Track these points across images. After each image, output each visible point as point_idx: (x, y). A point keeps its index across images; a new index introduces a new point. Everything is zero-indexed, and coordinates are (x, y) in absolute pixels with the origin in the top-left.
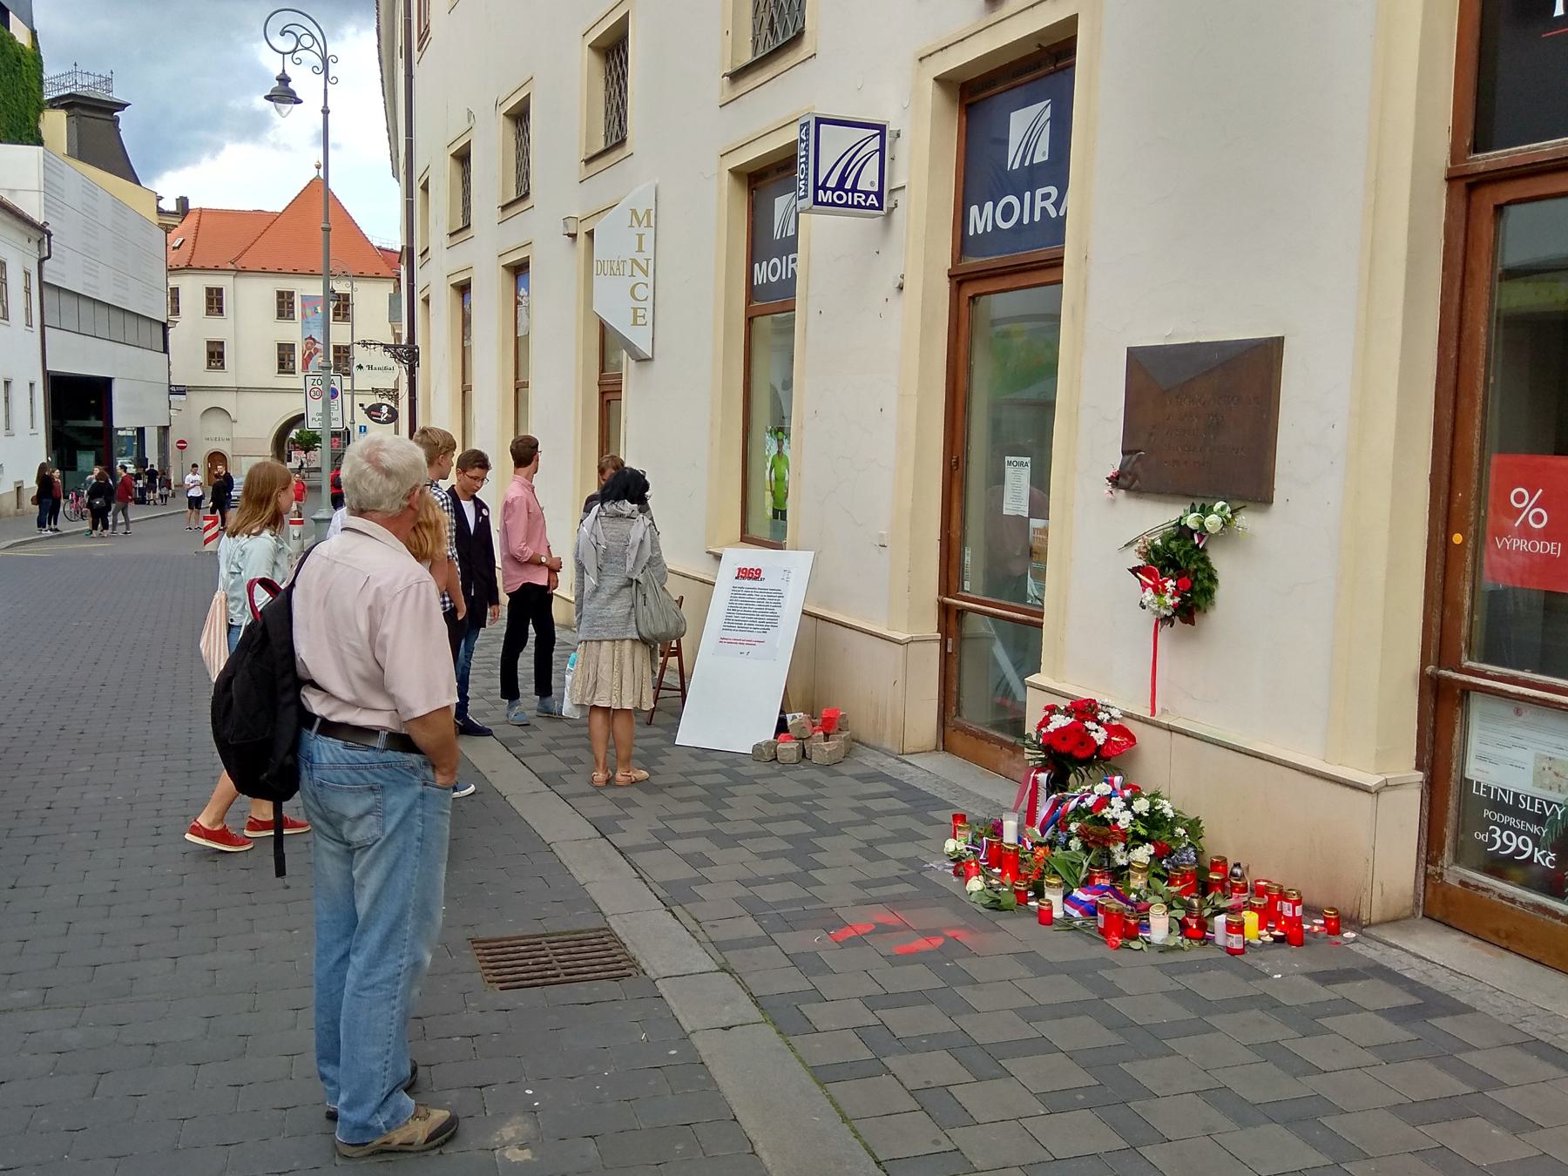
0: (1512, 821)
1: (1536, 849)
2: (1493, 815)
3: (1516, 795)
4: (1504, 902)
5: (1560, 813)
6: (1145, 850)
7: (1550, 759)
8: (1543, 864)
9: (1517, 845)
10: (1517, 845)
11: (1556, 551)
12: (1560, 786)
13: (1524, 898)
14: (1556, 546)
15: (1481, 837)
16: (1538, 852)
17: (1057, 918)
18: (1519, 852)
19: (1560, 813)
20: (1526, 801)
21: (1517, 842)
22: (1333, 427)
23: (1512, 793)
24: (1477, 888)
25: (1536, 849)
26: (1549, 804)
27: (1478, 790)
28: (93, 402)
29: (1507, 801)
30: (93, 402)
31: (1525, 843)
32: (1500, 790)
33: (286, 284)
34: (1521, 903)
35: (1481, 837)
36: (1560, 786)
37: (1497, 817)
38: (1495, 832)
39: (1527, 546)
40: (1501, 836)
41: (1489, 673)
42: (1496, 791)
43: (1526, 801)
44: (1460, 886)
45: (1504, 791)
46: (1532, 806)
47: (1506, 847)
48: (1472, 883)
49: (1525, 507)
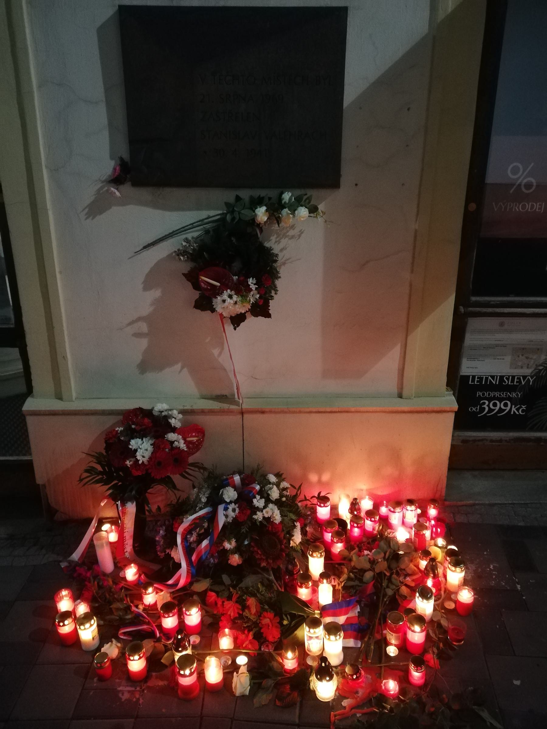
0: (497, 394)
1: (513, 406)
2: (483, 394)
3: (502, 377)
4: (494, 444)
5: (531, 381)
6: (278, 519)
7: (523, 349)
8: (517, 413)
9: (500, 407)
10: (500, 407)
11: (540, 209)
13: (507, 437)
14: (541, 205)
15: (474, 409)
16: (515, 407)
17: (79, 606)
18: (501, 410)
19: (531, 381)
20: (508, 379)
21: (500, 405)
22: (408, 109)
23: (498, 377)
24: (475, 441)
25: (513, 406)
26: (524, 377)
27: (473, 380)
28: (517, 683)
30: (517, 683)
31: (506, 405)
32: (490, 378)
33: (58, 405)
34: (506, 441)
35: (474, 409)
36: (528, 365)
37: (486, 394)
38: (484, 403)
39: (518, 208)
40: (488, 406)
41: (492, 303)
42: (487, 378)
43: (508, 380)
44: (462, 444)
45: (493, 377)
46: (513, 381)
47: (490, 410)
48: (471, 439)
49: (524, 178)
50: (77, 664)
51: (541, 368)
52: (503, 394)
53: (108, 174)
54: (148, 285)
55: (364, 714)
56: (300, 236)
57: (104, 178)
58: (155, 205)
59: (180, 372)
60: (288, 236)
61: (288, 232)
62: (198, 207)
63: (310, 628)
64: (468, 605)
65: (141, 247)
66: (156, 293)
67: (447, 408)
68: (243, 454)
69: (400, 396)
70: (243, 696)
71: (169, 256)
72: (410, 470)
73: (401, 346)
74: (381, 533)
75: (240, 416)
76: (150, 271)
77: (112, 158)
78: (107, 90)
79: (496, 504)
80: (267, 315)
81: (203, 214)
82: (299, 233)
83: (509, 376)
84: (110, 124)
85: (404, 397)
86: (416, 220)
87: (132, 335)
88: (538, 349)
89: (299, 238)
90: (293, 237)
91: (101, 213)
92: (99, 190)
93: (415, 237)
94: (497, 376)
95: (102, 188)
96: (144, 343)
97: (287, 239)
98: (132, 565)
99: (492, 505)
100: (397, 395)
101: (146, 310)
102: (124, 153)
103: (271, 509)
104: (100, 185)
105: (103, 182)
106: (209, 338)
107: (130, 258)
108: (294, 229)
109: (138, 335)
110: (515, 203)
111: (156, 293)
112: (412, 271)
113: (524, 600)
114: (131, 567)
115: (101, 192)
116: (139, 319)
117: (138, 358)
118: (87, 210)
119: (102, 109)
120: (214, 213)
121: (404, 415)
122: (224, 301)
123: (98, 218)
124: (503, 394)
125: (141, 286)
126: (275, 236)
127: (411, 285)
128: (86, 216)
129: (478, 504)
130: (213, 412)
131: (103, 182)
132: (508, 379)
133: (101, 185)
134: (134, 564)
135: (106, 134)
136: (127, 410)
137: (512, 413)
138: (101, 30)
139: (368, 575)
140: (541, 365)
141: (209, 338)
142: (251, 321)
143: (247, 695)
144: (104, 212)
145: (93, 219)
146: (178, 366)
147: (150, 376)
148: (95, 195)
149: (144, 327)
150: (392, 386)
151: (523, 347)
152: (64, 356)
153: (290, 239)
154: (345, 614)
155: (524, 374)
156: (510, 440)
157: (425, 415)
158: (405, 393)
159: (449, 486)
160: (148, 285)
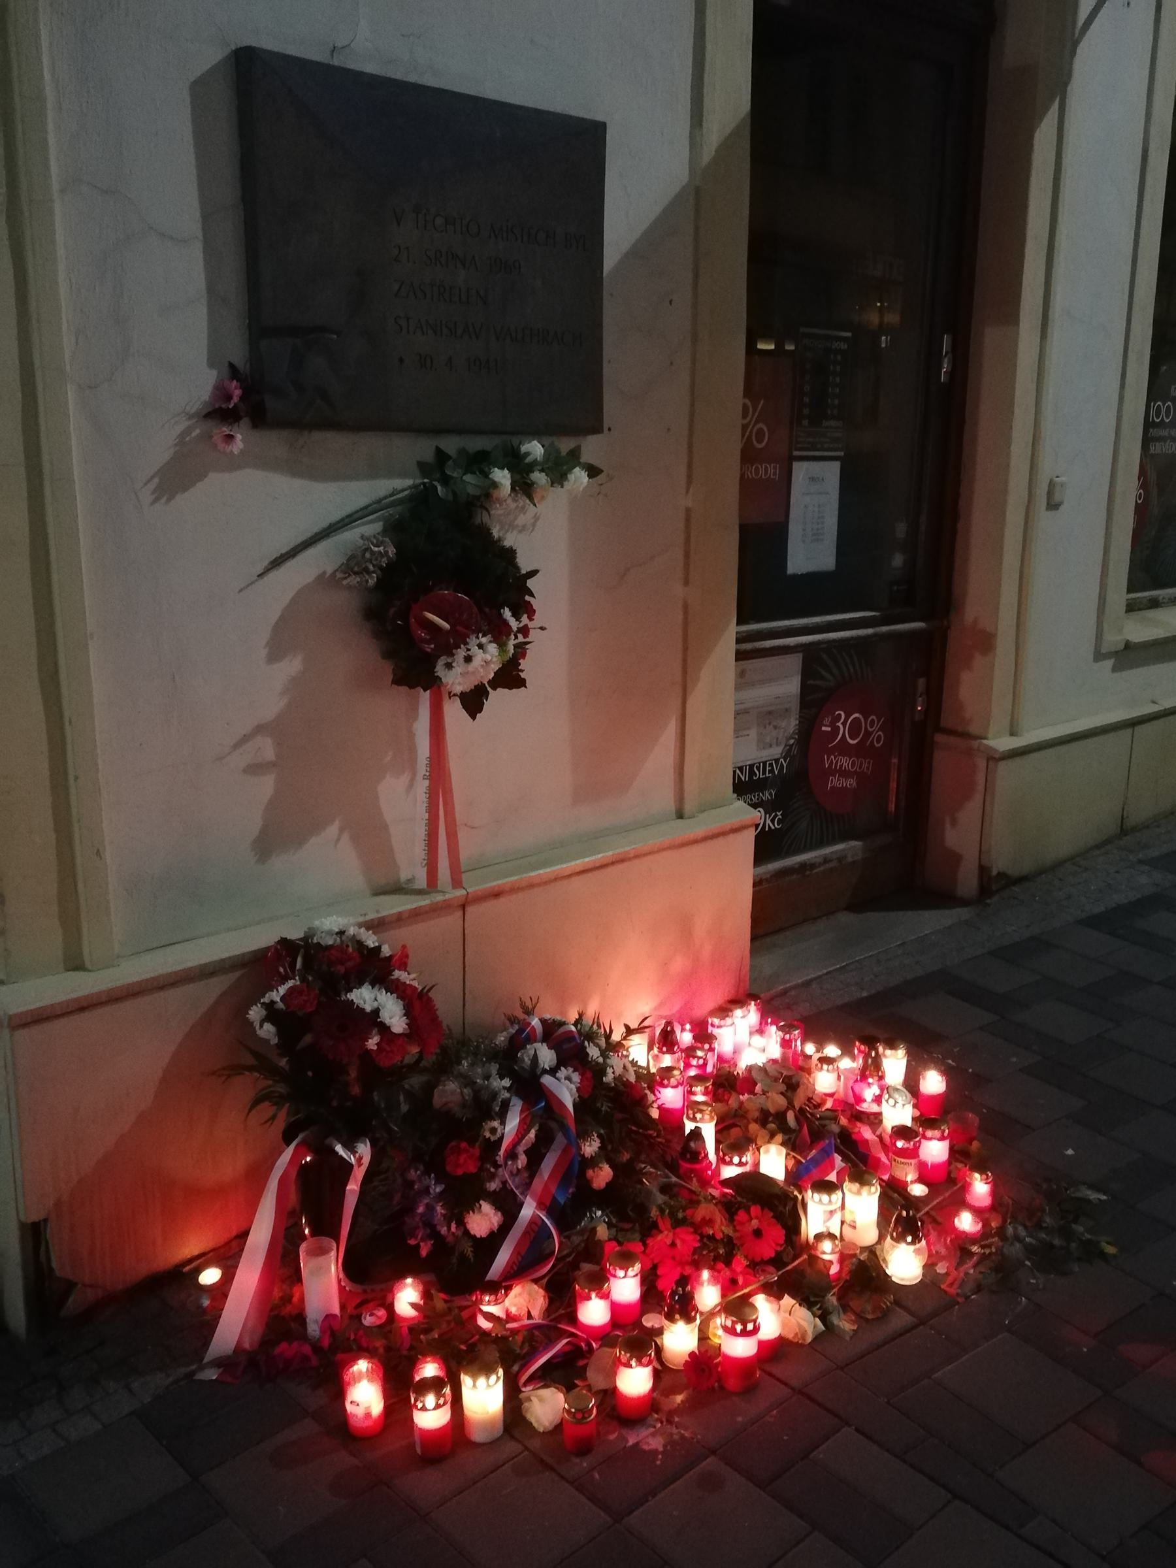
11: (775, 474)
12: (777, 739)
20: (758, 768)
22: (671, 302)
25: (768, 816)
26: (777, 761)
29: (743, 779)
30: (1070, 1152)
34: (766, 880)
50: (508, 1461)
51: (792, 741)
52: (754, 797)
53: (203, 399)
54: (276, 653)
55: (975, 1266)
56: (534, 525)
57: (193, 411)
58: (293, 468)
59: (338, 840)
60: (517, 526)
61: (515, 519)
62: (373, 471)
63: (829, 1195)
64: (940, 1095)
65: (266, 563)
66: (292, 666)
67: (735, 821)
68: (464, 999)
69: (680, 815)
70: (818, 1338)
71: (321, 578)
72: (707, 951)
73: (676, 720)
74: (691, 1087)
75: (460, 913)
76: (282, 618)
77: (211, 365)
78: (206, 218)
79: (811, 980)
80: (521, 683)
81: (384, 487)
82: (532, 521)
83: (759, 763)
84: (211, 289)
85: (686, 816)
86: (687, 492)
87: (245, 771)
88: (787, 710)
89: (533, 530)
90: (523, 529)
91: (185, 489)
92: (182, 435)
93: (688, 520)
94: (746, 766)
95: (187, 431)
96: (266, 786)
97: (515, 532)
98: (409, 1281)
99: (807, 984)
100: (674, 815)
101: (271, 706)
102: (237, 354)
103: (565, 1079)
104: (185, 424)
105: (191, 417)
106: (390, 753)
107: (241, 591)
108: (524, 514)
109: (255, 769)
110: (772, 465)
111: (292, 666)
112: (686, 582)
113: (972, 1072)
114: (405, 1286)
115: (187, 439)
116: (259, 729)
117: (254, 823)
118: (156, 480)
119: (196, 252)
120: (402, 484)
121: (696, 849)
122: (468, 659)
123: (181, 499)
124: (754, 797)
125: (264, 653)
126: (498, 527)
127: (686, 608)
128: (154, 496)
129: (791, 988)
130: (417, 915)
131: (191, 417)
132: (758, 768)
133: (187, 423)
134: (414, 1277)
135: (202, 311)
136: (255, 951)
137: (767, 829)
138: (199, 88)
139: (791, 1117)
140: (791, 738)
141: (390, 753)
142: (497, 698)
143: (824, 1331)
144: (193, 484)
145: (169, 500)
146: (333, 830)
147: (279, 863)
148: (176, 445)
149: (267, 748)
150: (665, 800)
151: (770, 709)
152: (98, 850)
153: (520, 532)
154: (833, 1170)
155: (739, 765)
156: (771, 876)
157: (721, 841)
158: (688, 807)
159: (753, 967)
160: (276, 653)
